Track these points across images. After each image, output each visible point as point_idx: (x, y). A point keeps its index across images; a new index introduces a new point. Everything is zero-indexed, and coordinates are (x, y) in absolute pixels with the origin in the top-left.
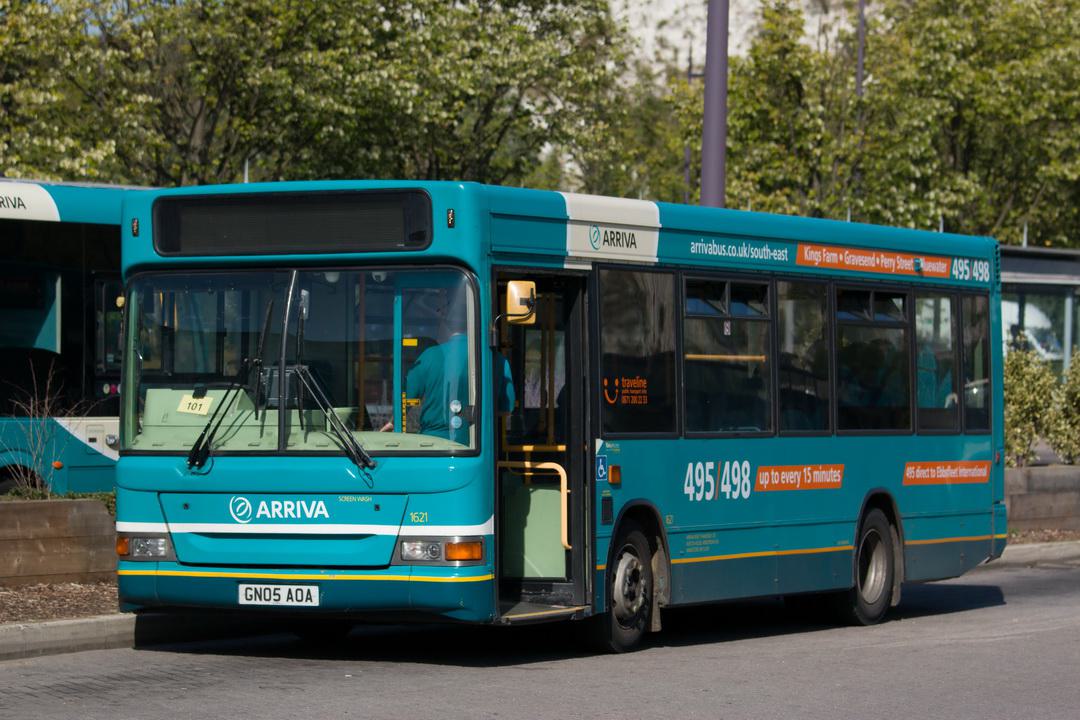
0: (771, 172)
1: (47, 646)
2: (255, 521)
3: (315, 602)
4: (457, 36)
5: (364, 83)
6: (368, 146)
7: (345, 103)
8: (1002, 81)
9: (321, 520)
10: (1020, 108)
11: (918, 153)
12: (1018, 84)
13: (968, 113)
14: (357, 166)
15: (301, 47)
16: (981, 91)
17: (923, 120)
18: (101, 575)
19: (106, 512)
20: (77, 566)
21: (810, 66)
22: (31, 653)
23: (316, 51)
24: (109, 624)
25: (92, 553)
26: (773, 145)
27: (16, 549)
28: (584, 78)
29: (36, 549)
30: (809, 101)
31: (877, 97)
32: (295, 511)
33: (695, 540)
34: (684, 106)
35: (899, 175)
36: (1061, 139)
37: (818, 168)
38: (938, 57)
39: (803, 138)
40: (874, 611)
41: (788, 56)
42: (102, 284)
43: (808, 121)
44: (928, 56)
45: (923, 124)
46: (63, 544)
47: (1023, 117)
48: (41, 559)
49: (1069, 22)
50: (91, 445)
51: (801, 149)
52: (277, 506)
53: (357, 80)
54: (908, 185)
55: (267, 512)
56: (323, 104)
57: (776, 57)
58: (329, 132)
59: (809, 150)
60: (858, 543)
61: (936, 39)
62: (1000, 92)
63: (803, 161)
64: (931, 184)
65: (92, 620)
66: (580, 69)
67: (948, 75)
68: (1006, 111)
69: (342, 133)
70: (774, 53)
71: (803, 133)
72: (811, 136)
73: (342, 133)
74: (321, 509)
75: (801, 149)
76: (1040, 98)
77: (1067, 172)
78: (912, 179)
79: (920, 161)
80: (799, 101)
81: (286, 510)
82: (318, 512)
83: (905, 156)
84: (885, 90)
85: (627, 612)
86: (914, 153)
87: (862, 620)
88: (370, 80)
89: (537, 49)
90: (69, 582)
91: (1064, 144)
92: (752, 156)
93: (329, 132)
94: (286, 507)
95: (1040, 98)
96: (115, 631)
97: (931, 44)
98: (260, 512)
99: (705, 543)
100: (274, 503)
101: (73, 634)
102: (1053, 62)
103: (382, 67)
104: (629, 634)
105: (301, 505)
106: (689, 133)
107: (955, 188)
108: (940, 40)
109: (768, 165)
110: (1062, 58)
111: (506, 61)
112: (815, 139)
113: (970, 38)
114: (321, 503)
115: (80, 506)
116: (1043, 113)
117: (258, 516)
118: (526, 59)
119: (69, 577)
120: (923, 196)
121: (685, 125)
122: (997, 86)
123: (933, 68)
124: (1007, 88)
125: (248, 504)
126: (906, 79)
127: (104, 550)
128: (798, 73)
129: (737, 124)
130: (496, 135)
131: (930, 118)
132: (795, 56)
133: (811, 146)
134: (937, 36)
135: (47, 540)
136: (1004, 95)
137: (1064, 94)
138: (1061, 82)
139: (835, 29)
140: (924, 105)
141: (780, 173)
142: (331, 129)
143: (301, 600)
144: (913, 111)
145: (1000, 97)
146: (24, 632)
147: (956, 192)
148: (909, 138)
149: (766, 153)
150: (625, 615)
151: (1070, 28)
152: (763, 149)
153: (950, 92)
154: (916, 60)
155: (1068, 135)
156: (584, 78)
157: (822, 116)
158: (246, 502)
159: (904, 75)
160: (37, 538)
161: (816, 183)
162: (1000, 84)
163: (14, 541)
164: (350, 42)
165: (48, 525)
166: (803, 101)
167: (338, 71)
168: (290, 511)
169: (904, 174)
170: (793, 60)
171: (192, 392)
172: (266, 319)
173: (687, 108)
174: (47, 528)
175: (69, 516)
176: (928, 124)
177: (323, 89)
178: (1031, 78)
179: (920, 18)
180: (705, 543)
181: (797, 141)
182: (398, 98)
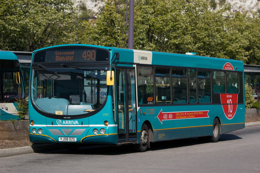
0: (108, 43)
1: (15, 153)
2: (62, 125)
3: (76, 141)
4: (40, 12)
5: (21, 23)
6: (21, 39)
7: (17, 28)
8: (160, 20)
9: (77, 124)
11: (142, 38)
12: (163, 20)
13: (152, 28)
14: (19, 43)
15: (6, 15)
16: (155, 23)
17: (143, 30)
18: (12, 138)
20: (7, 136)
21: (117, 17)
22: (13, 155)
23: (10, 16)
24: (26, 148)
25: (10, 133)
26: (108, 36)
28: (69, 21)
30: (116, 26)
32: (71, 123)
34: (87, 27)
35: (138, 43)
36: (174, 34)
37: (119, 42)
39: (115, 35)
40: (217, 139)
42: (4, 73)
44: (144, 15)
45: (143, 31)
46: (4, 131)
50: (3, 109)
51: (114, 37)
52: (67, 122)
53: (20, 23)
54: (140, 45)
55: (65, 123)
56: (12, 28)
58: (13, 35)
59: (116, 37)
60: (213, 125)
61: (145, 11)
62: (160, 23)
63: (115, 40)
64: (145, 45)
65: (23, 148)
66: (68, 19)
68: (161, 28)
69: (16, 35)
70: (108, 14)
71: (115, 33)
72: (117, 34)
73: (16, 35)
74: (77, 122)
75: (114, 37)
76: (169, 24)
77: (176, 42)
78: (140, 44)
79: (142, 40)
80: (114, 26)
81: (69, 123)
82: (76, 123)
83: (139, 39)
85: (144, 143)
86: (141, 38)
87: (215, 142)
88: (23, 23)
89: (58, 15)
90: (6, 140)
91: (175, 35)
92: (103, 39)
93: (13, 35)
94: (69, 122)
95: (169, 24)
96: (27, 150)
97: (144, 12)
98: (63, 123)
99: (162, 135)
100: (66, 121)
101: (20, 151)
103: (25, 20)
104: (144, 148)
105: (72, 122)
106: (88, 34)
107: (150, 46)
109: (107, 41)
111: (51, 18)
112: (118, 35)
113: (153, 10)
114: (77, 121)
115: (7, 123)
117: (63, 124)
119: (6, 139)
120: (143, 48)
121: (87, 32)
122: (159, 22)
123: (145, 18)
124: (162, 22)
125: (61, 121)
126: (139, 20)
127: (12, 133)
128: (114, 19)
129: (99, 31)
130: (48, 35)
131: (144, 29)
133: (117, 36)
134: (146, 10)
136: (161, 24)
137: (175, 23)
139: (98, 5)
140: (143, 26)
141: (110, 43)
142: (13, 34)
144: (140, 28)
145: (160, 24)
146: (11, 151)
147: (150, 47)
148: (140, 34)
149: (106, 38)
150: (144, 143)
151: (175, 7)
152: (106, 37)
153: (149, 23)
154: (141, 16)
155: (176, 33)
156: (69, 21)
157: (119, 29)
158: (60, 121)
159: (138, 19)
161: (118, 45)
162: (160, 21)
164: (18, 14)
166: (115, 26)
167: (16, 21)
168: (70, 123)
169: (139, 43)
170: (113, 16)
171: (48, 98)
173: (87, 28)
176: (144, 31)
177: (12, 25)
180: (162, 135)
182: (29, 27)
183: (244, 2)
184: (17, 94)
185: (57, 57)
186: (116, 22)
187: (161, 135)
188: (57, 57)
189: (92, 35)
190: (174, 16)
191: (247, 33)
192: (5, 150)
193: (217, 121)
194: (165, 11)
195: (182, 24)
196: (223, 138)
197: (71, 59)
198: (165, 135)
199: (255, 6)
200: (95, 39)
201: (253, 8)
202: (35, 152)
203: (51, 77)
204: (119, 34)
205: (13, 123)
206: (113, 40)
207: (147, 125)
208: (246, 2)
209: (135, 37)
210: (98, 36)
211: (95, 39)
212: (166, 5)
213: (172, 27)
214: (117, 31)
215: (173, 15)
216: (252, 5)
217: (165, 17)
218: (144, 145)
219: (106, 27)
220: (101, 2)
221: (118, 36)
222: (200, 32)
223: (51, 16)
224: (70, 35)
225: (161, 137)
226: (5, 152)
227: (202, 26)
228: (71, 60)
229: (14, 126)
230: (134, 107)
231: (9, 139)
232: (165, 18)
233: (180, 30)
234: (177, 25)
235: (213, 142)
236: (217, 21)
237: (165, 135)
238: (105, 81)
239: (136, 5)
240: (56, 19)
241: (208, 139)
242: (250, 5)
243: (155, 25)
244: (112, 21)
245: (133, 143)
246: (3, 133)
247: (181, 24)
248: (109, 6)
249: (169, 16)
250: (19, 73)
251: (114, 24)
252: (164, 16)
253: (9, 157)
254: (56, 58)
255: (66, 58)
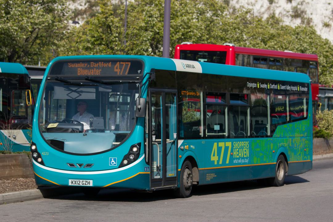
10: (173, 35)
16: (161, 29)
18: (26, 176)
19: (28, 158)
25: (24, 169)
26: (103, 46)
27: (7, 168)
29: (11, 168)
31: (133, 31)
33: (209, 175)
38: (150, 19)
41: (108, 19)
43: (113, 39)
45: (147, 39)
47: (174, 37)
48: (13, 171)
49: (186, 8)
50: (9, 138)
51: (111, 47)
57: (104, 19)
59: (113, 48)
60: (277, 162)
67: (154, 24)
70: (103, 18)
75: (111, 47)
84: (135, 29)
99: (212, 176)
102: (183, 21)
104: (188, 193)
108: (151, 14)
110: (186, 19)
111: (38, 21)
115: (22, 156)
116: (180, 36)
118: (44, 20)
126: (141, 26)
128: (111, 24)
132: (110, 19)
133: (114, 46)
134: (150, 13)
135: (14, 165)
138: (186, 27)
143: (84, 184)
151: (187, 10)
152: (100, 47)
153: (154, 30)
154: (144, 20)
160: (12, 165)
163: (6, 166)
165: (14, 161)
172: (152, 115)
174: (14, 162)
175: (19, 159)
178: (177, 25)
179: (143, 7)
180: (212, 176)
181: (110, 45)
183: (252, 5)
184: (27, 118)
185: (79, 70)
186: (114, 29)
187: (210, 175)
188: (79, 70)
189: (83, 44)
190: (186, 21)
191: (273, 43)
192: (32, 192)
193: (283, 157)
194: (174, 14)
195: (195, 31)
196: (289, 180)
197: (91, 71)
198: (216, 176)
199: (266, 10)
200: (87, 49)
201: (263, 13)
202: (45, 197)
203: (69, 95)
204: (117, 43)
205: (28, 156)
206: (109, 51)
207: (191, 162)
208: (255, 5)
209: (137, 47)
210: (90, 46)
211: (87, 49)
212: (175, 7)
213: (183, 35)
214: (114, 40)
215: (185, 20)
216: (263, 10)
217: (174, 22)
218: (187, 189)
219: (101, 34)
220: (73, 3)
221: (116, 46)
222: (216, 42)
223: (38, 18)
224: (61, 43)
225: (210, 179)
226: (31, 194)
227: (219, 34)
228: (97, 74)
229: (30, 161)
230: (175, 138)
231: (23, 177)
232: (175, 24)
233: (194, 38)
234: (189, 33)
235: (276, 186)
236: (235, 29)
237: (216, 176)
238: (230, 98)
239: (137, 7)
240: (43, 22)
241: (270, 182)
242: (259, 10)
243: (161, 32)
244: (109, 27)
245: (172, 187)
246: (16, 169)
247: (194, 31)
248: (104, 7)
249: (179, 21)
250: (30, 90)
251: (111, 31)
252: (173, 21)
253: (33, 201)
254: (79, 72)
255: (91, 71)
